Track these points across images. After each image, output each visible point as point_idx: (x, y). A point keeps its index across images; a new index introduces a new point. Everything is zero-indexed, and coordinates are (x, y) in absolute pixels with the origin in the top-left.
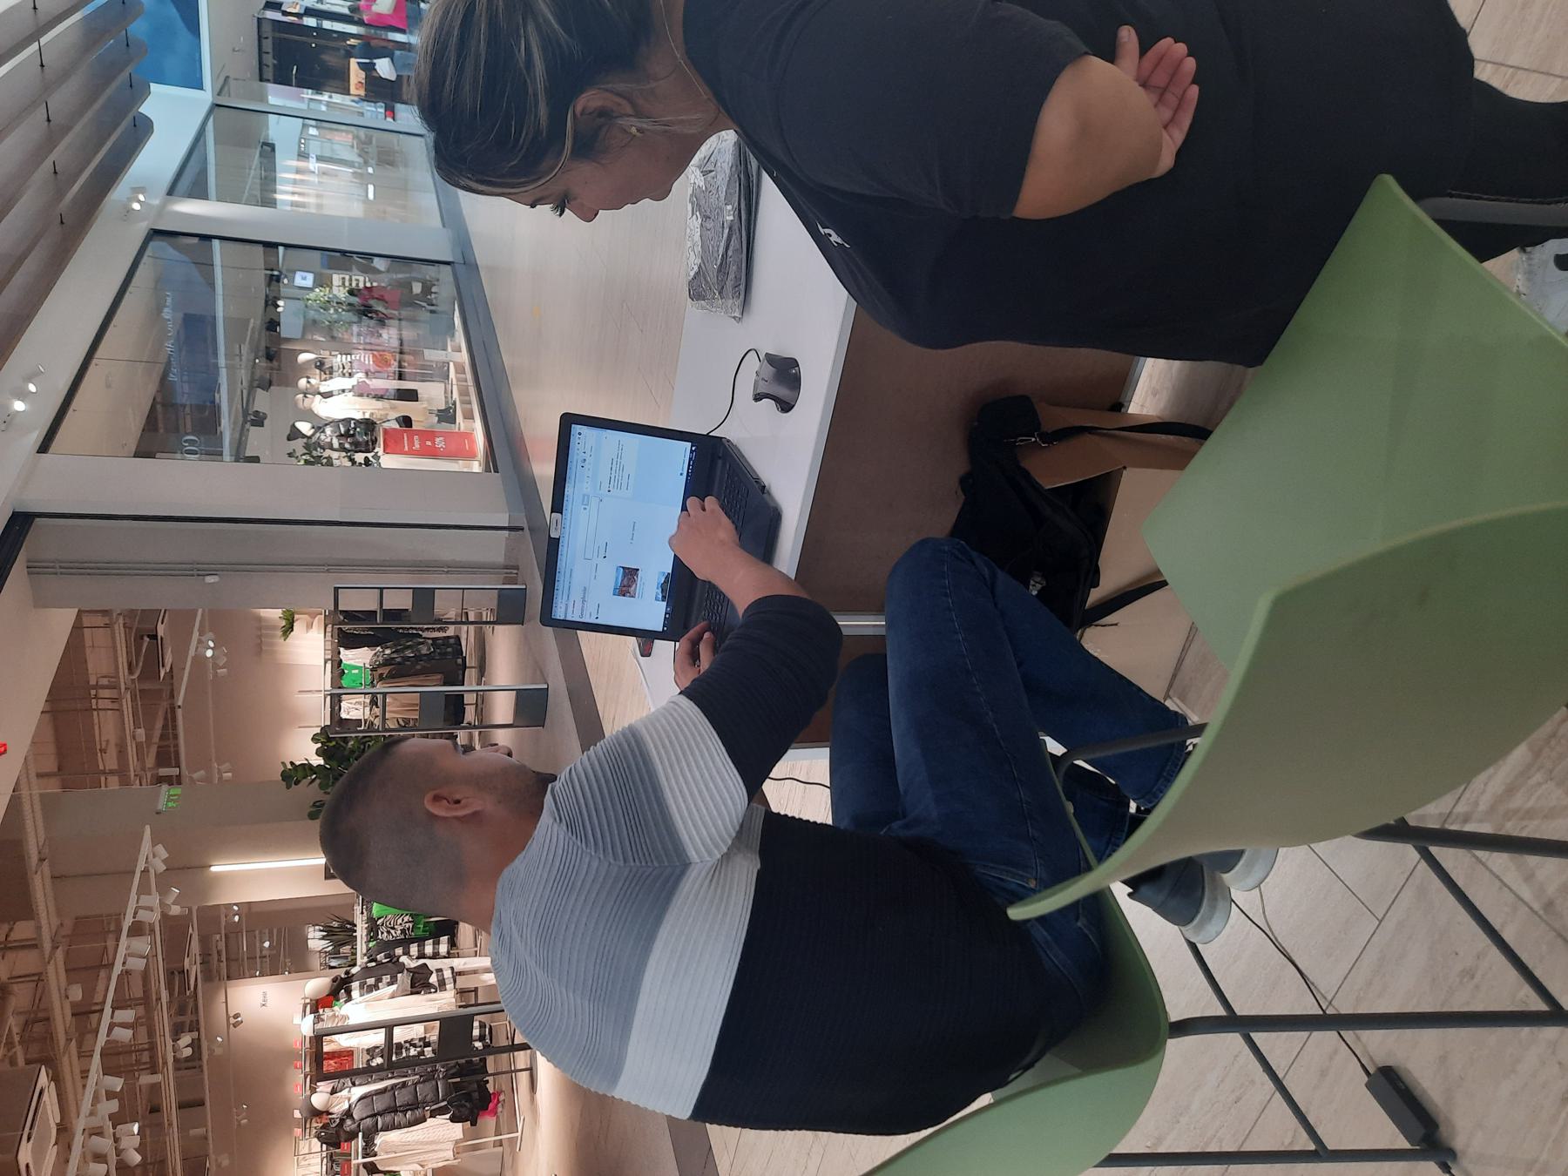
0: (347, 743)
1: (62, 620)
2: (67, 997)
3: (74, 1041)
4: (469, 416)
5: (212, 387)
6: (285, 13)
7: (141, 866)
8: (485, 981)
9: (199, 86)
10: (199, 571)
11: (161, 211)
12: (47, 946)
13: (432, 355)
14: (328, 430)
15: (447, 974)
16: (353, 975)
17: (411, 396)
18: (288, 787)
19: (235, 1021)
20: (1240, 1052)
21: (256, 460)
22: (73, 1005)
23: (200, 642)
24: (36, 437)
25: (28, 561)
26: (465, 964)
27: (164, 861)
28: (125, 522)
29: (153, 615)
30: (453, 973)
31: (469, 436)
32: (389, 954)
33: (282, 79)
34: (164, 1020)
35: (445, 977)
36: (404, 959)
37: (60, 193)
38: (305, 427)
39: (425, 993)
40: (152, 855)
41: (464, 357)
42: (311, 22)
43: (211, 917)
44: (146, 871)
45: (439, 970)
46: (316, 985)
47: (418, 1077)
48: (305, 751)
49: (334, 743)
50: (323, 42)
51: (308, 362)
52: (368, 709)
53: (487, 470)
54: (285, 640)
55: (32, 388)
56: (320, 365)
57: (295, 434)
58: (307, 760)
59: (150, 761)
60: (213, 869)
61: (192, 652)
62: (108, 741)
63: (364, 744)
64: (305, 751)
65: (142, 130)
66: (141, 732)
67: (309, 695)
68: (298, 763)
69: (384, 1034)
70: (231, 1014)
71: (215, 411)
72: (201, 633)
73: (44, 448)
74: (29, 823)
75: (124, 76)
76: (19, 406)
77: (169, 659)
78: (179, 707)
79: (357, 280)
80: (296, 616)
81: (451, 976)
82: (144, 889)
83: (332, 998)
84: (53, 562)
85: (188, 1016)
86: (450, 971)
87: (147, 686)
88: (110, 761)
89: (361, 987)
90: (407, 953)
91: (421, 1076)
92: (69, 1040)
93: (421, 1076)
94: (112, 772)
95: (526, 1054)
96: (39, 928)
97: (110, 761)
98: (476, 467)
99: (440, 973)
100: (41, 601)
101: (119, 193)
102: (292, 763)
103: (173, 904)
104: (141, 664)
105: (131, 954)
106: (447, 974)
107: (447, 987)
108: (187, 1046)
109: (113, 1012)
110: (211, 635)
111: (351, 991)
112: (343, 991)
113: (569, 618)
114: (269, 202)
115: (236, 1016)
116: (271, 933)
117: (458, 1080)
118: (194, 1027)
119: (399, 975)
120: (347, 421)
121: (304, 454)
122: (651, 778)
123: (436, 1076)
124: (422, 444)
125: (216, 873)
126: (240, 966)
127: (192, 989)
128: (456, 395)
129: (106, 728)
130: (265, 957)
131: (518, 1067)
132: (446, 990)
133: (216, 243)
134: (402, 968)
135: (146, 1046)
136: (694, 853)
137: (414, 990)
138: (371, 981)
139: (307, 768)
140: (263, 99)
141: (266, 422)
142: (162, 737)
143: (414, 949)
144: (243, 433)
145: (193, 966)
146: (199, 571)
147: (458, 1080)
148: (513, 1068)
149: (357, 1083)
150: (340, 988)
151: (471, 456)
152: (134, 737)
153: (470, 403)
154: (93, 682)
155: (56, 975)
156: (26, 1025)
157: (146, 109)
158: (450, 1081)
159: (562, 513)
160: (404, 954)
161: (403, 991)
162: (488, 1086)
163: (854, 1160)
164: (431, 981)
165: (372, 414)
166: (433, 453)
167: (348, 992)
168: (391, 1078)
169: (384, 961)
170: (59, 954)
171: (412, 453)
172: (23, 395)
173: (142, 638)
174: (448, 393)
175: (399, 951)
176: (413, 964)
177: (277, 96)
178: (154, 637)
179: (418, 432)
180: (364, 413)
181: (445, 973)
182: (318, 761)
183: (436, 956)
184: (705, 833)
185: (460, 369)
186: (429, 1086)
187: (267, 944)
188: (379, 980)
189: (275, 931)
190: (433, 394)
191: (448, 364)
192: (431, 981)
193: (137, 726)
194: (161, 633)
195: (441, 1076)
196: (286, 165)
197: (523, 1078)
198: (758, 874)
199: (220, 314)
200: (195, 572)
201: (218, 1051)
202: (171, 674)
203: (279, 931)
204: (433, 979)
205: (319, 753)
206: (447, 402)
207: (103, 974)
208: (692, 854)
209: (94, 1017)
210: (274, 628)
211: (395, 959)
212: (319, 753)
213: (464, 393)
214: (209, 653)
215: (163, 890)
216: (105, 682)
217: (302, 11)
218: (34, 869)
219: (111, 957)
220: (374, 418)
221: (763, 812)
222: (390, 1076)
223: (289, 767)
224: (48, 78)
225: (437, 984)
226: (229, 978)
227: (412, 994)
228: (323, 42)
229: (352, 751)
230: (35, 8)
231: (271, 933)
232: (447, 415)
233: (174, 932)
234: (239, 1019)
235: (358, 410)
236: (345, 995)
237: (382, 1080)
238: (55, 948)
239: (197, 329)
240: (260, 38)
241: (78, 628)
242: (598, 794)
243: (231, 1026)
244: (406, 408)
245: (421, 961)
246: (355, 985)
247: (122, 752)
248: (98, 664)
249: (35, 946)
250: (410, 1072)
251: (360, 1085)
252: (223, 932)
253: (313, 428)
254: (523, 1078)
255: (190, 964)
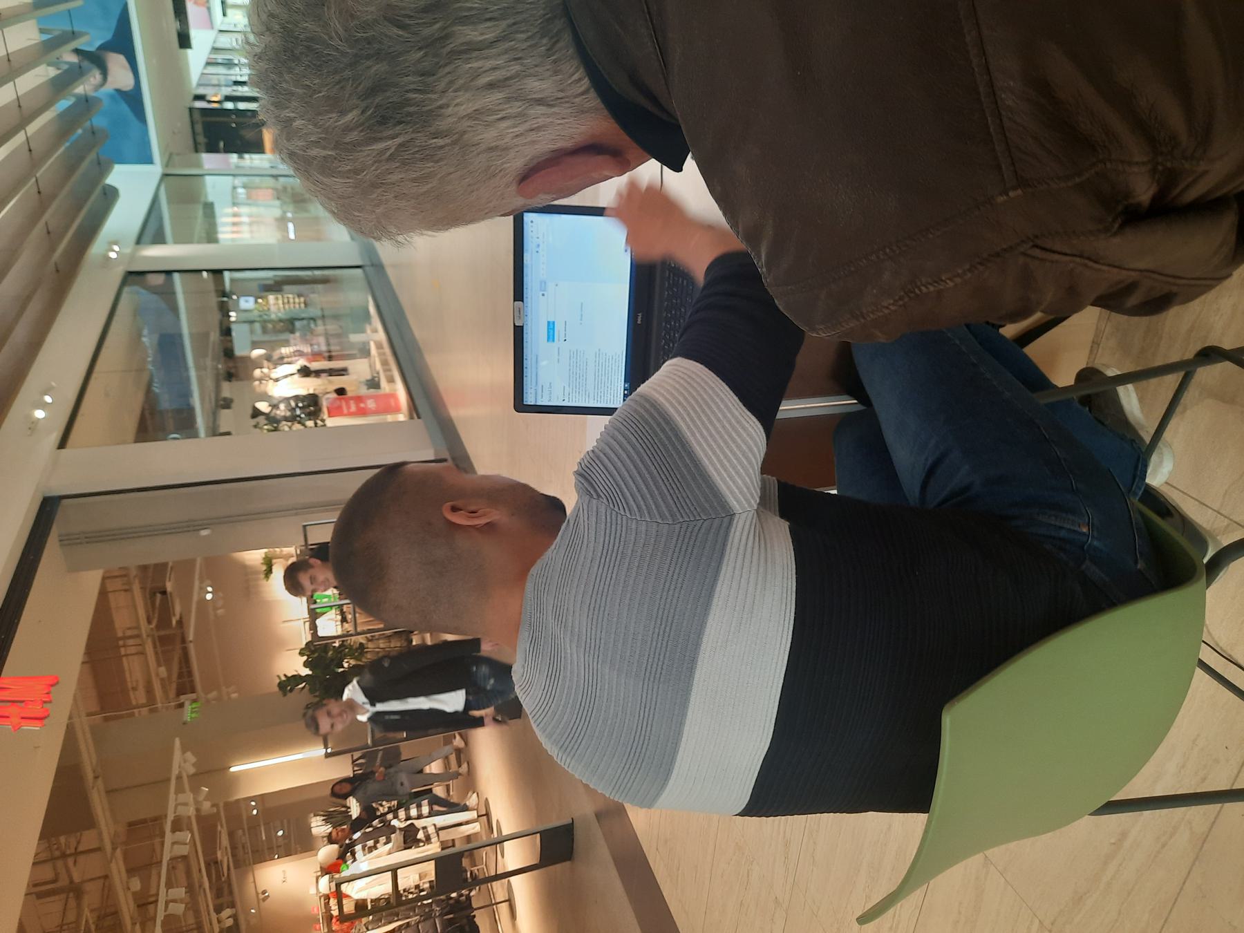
0: (327, 653)
1: (92, 580)
2: (129, 889)
3: (138, 925)
4: (391, 380)
5: (187, 394)
6: (210, 102)
7: (175, 772)
8: (462, 833)
9: (149, 160)
10: (192, 527)
11: (132, 257)
12: (108, 847)
13: (355, 338)
14: (282, 406)
15: (431, 830)
16: (356, 840)
17: (342, 372)
18: (285, 695)
19: (264, 896)
20: (1198, 735)
21: (228, 434)
22: (134, 894)
23: (201, 588)
24: (55, 437)
25: (59, 536)
26: (444, 820)
27: (194, 765)
28: (132, 494)
29: (161, 568)
30: (436, 828)
31: (393, 396)
32: (382, 820)
33: (212, 148)
34: (207, 899)
35: (430, 832)
36: (395, 823)
37: (52, 249)
38: (263, 406)
39: (416, 848)
40: (183, 762)
41: (381, 336)
42: (229, 105)
43: (234, 810)
44: (179, 778)
45: (424, 828)
46: (327, 852)
47: (418, 917)
48: (296, 665)
49: (316, 655)
50: (241, 120)
51: (261, 356)
52: (339, 627)
53: (411, 418)
54: (267, 581)
55: (48, 399)
56: (268, 358)
57: (256, 413)
58: (297, 671)
59: (172, 694)
60: (232, 769)
61: (195, 598)
62: (137, 681)
63: (341, 652)
64: (296, 665)
65: (111, 195)
66: (163, 671)
67: (292, 623)
68: (289, 675)
69: (390, 875)
70: (260, 891)
71: (191, 410)
72: (202, 581)
73: (62, 444)
74: (83, 747)
75: (92, 156)
76: (39, 414)
77: (178, 609)
78: (191, 642)
79: (288, 298)
80: (274, 561)
81: (434, 831)
82: (179, 790)
83: (340, 861)
84: (79, 534)
85: (225, 894)
86: (433, 827)
87: (162, 633)
88: (139, 697)
89: (363, 848)
90: (396, 817)
91: (421, 916)
92: (134, 924)
93: (421, 916)
94: (143, 706)
95: (502, 885)
96: (100, 834)
97: (139, 697)
98: (401, 417)
99: (425, 830)
100: (75, 567)
101: (96, 248)
102: (285, 675)
103: (205, 800)
104: (156, 615)
105: (175, 844)
106: (431, 830)
107: (433, 840)
108: (229, 917)
109: (167, 892)
110: (208, 582)
111: (355, 853)
112: (349, 854)
113: (539, 403)
114: (211, 237)
115: (264, 892)
116: (282, 822)
117: (451, 916)
118: (232, 905)
119: (393, 836)
120: (297, 398)
121: (266, 425)
122: (676, 435)
123: (433, 914)
124: (358, 407)
125: (233, 772)
126: (264, 853)
127: (226, 875)
128: (378, 366)
129: (133, 670)
130: (280, 846)
131: (498, 901)
132: (431, 843)
133: (176, 276)
134: (393, 830)
135: (194, 926)
136: (735, 503)
137: (407, 846)
138: (370, 843)
139: (297, 679)
140: (199, 165)
141: (233, 405)
142: (180, 676)
143: (402, 814)
144: (215, 415)
145: (223, 856)
146: (192, 527)
147: (451, 916)
148: (493, 902)
149: (370, 928)
150: (346, 852)
151: (397, 410)
152: (157, 675)
153: (390, 370)
154: (120, 634)
155: (118, 869)
156: (100, 918)
157: (111, 180)
158: (446, 917)
159: (523, 301)
160: (394, 818)
161: (398, 847)
162: (475, 919)
163: (816, 916)
164: (419, 837)
165: (315, 390)
166: (362, 412)
167: (353, 854)
168: (397, 921)
169: (379, 826)
170: (119, 852)
171: (350, 414)
172: (43, 406)
173: (154, 594)
174: (372, 366)
175: (390, 816)
176: (403, 825)
177: (209, 161)
178: (164, 593)
179: (352, 398)
180: (308, 390)
181: (429, 829)
182: (306, 672)
183: (420, 817)
184: (740, 482)
185: (379, 346)
186: (429, 923)
187: (280, 833)
188: (377, 842)
189: (285, 821)
190: (359, 369)
191: (369, 343)
192: (419, 837)
193: (159, 665)
194: (169, 587)
195: (437, 914)
196: (224, 217)
197: (503, 909)
198: (789, 528)
199: (185, 331)
200: (191, 528)
201: (253, 921)
202: (180, 622)
203: (289, 822)
204: (421, 835)
205: (306, 664)
206: (371, 370)
207: (154, 872)
208: (733, 503)
209: (151, 907)
210: (257, 572)
211: (387, 823)
212: (306, 664)
213: (385, 363)
214: (209, 596)
215: (195, 790)
216: (129, 633)
217: (223, 98)
218: (91, 785)
219: (159, 857)
220: (317, 392)
221: (776, 482)
222: (396, 919)
223: (283, 678)
224: (33, 157)
225: (424, 839)
226: (254, 864)
227: (405, 849)
228: (241, 120)
229: (332, 660)
230: (20, 106)
231: (282, 822)
232: (373, 384)
233: (207, 826)
234: (267, 894)
235: (303, 388)
236: (351, 858)
237: (390, 923)
238: (114, 849)
239: (169, 345)
240: (193, 123)
241: (103, 594)
242: (628, 461)
243: (261, 901)
244: (338, 382)
245: (409, 822)
246: (358, 848)
247: (149, 691)
248: (121, 621)
249: (98, 849)
250: (411, 914)
251: (373, 929)
252: (246, 827)
253: (270, 406)
254: (503, 909)
255: (222, 856)
